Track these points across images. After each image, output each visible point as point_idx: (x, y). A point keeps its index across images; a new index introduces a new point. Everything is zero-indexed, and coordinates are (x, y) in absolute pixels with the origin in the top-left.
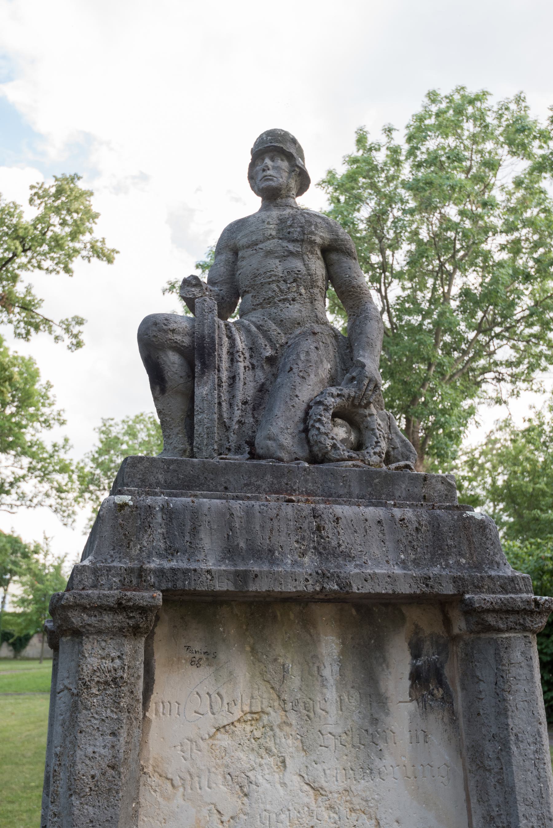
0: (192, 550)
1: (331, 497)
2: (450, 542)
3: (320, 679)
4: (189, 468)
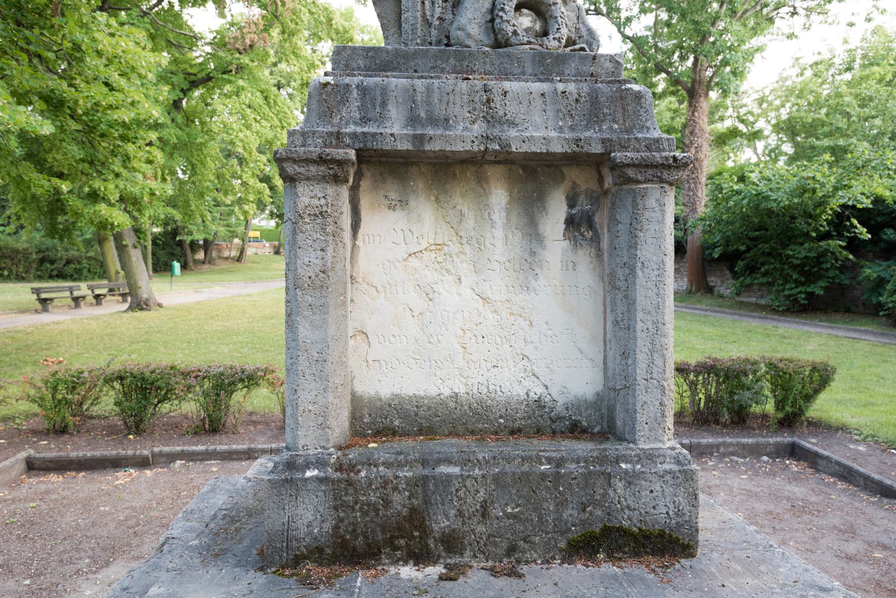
0: (381, 119)
1: (505, 75)
2: (606, 111)
3: (490, 222)
4: (384, 54)
